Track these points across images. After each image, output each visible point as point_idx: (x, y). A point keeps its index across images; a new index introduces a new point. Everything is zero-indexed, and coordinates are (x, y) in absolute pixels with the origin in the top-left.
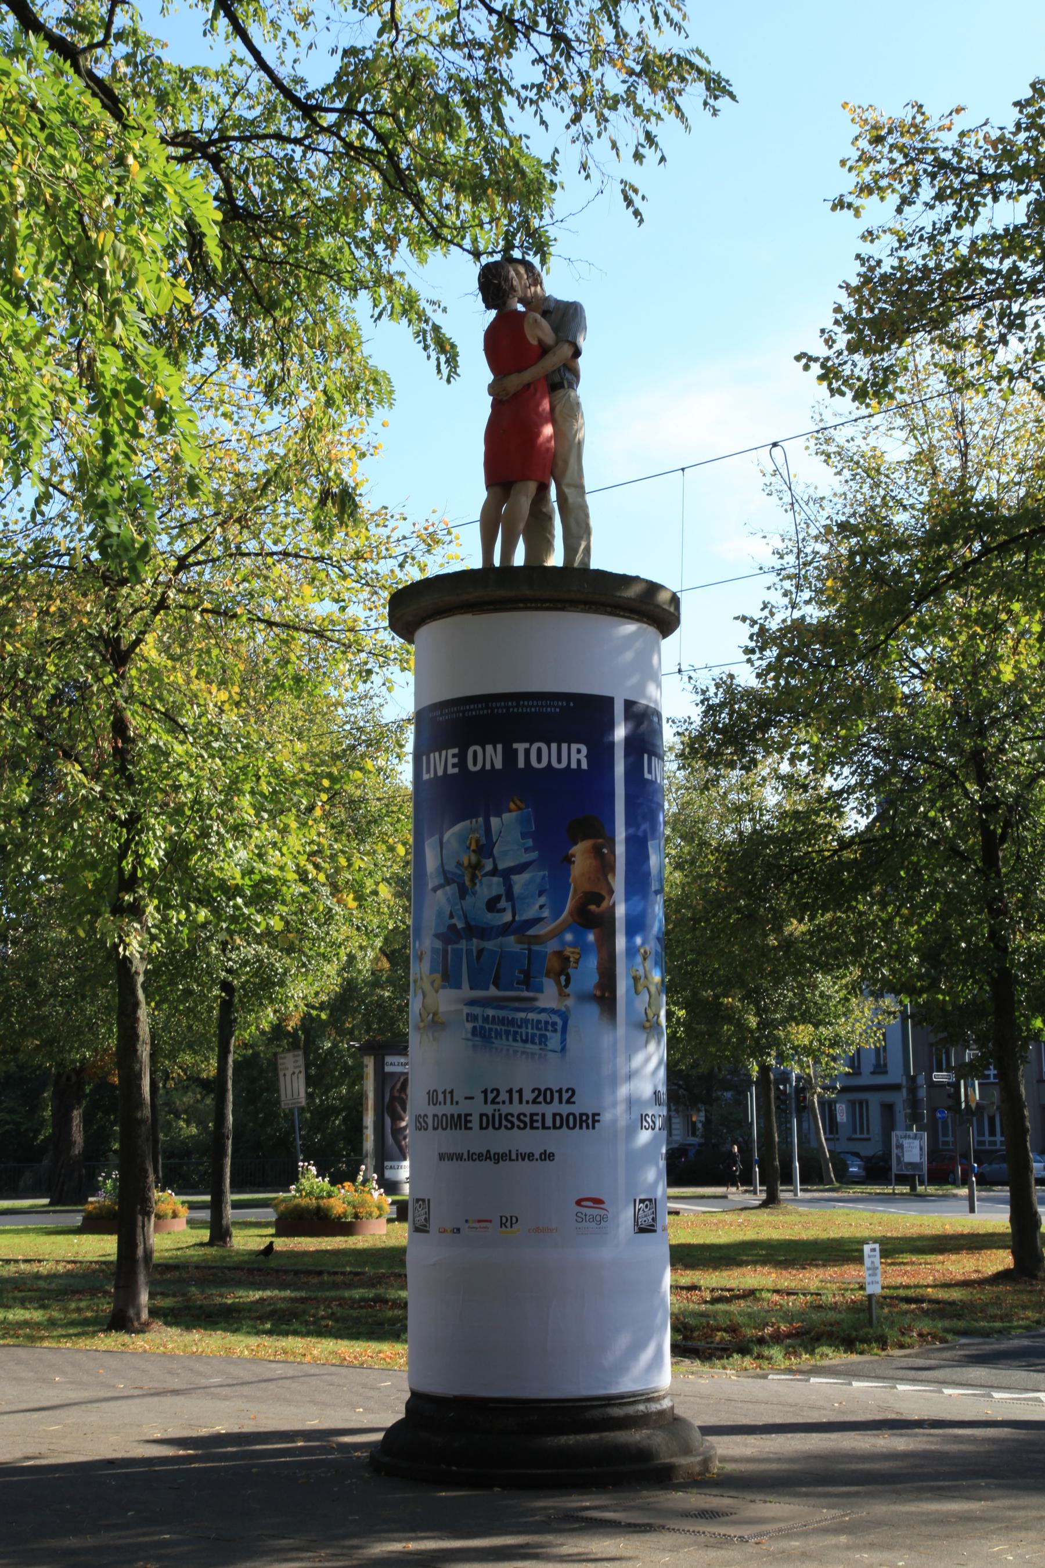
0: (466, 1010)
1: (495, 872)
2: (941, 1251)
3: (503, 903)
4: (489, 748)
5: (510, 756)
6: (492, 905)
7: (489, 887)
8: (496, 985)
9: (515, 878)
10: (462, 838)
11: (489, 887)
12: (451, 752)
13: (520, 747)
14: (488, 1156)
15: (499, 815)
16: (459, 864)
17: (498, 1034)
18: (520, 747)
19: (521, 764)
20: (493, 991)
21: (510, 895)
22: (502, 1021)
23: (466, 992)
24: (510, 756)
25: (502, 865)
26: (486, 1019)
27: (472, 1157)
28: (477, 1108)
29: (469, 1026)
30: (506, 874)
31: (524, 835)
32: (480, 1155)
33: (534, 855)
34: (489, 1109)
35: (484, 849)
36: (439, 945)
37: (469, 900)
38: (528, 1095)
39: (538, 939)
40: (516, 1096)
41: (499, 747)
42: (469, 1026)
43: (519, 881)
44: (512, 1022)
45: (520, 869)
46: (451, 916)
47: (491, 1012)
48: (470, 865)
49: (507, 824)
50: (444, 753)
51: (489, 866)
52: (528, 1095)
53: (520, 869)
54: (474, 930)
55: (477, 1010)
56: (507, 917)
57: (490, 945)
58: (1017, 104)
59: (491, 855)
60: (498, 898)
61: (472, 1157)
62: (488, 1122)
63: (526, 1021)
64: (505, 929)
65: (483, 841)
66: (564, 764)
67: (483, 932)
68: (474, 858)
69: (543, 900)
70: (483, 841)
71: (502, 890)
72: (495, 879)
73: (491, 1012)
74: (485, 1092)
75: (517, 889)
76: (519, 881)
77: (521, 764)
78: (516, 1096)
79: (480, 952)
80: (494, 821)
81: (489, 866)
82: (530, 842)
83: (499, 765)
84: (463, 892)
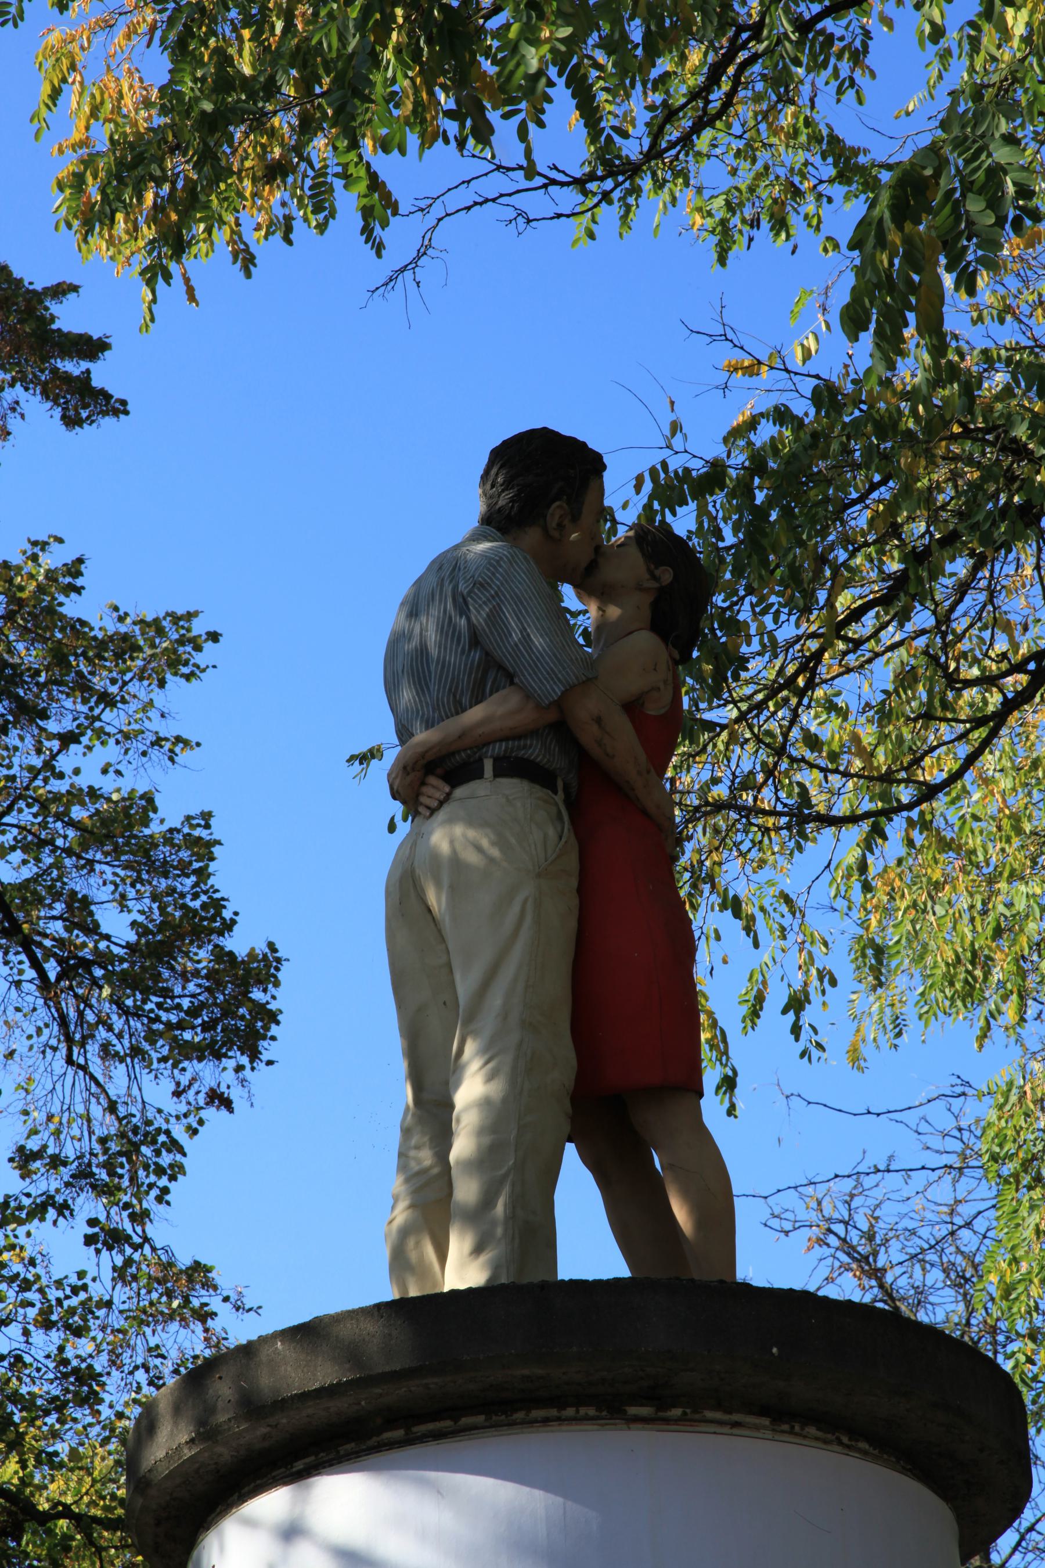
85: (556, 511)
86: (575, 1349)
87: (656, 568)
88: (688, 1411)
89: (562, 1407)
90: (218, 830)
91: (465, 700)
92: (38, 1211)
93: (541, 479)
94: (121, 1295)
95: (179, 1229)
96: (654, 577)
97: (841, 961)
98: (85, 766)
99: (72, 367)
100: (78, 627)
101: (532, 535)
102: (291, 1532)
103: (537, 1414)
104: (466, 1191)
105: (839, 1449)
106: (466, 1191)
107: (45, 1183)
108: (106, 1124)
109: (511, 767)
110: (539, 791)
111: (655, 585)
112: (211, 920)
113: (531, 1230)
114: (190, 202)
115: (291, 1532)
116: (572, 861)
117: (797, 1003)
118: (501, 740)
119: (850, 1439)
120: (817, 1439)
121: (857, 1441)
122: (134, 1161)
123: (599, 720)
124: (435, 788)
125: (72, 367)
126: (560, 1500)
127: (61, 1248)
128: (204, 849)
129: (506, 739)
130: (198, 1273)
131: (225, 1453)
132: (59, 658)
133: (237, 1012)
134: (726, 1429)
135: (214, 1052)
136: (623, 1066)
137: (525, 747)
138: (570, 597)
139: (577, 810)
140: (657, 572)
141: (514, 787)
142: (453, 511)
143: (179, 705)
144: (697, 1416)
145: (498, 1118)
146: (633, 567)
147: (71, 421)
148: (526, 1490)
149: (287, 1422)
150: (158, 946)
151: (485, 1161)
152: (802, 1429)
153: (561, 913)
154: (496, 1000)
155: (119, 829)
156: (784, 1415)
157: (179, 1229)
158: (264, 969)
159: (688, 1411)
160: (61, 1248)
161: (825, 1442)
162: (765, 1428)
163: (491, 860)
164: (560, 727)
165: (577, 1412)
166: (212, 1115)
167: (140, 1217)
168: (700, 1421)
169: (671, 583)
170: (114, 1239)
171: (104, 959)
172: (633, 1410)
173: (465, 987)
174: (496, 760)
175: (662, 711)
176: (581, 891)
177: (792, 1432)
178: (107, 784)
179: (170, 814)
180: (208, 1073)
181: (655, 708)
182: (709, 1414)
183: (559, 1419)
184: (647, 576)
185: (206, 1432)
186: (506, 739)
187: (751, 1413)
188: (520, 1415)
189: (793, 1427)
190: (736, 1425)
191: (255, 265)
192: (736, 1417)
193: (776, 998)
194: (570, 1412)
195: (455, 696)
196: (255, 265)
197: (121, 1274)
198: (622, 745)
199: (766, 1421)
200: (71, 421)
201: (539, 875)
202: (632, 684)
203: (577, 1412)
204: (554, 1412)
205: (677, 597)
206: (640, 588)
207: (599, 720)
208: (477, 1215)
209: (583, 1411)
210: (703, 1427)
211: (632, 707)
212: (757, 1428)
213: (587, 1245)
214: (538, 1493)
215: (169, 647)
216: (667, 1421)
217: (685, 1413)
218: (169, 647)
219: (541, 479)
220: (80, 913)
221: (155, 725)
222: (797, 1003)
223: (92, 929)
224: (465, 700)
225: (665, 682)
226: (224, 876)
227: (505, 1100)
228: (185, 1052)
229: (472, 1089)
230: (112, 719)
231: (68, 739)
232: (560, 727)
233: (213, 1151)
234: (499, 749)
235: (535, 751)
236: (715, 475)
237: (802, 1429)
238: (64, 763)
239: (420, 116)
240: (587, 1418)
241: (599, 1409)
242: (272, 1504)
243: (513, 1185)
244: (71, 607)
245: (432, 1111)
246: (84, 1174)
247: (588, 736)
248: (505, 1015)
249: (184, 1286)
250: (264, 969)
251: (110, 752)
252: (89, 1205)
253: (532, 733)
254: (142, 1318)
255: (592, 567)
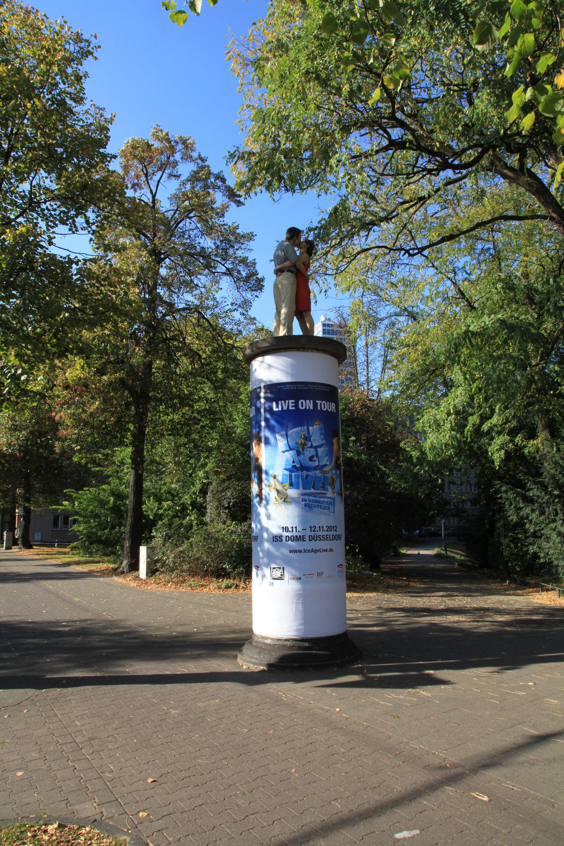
0: (302, 497)
1: (311, 447)
2: (41, 579)
3: (315, 459)
4: (308, 401)
5: (315, 405)
6: (311, 459)
7: (309, 452)
8: (314, 488)
9: (319, 449)
10: (297, 433)
11: (309, 452)
12: (291, 401)
13: (319, 402)
14: (312, 551)
15: (312, 426)
16: (297, 443)
17: (315, 506)
18: (319, 402)
19: (319, 409)
20: (312, 491)
21: (317, 456)
22: (316, 501)
23: (301, 490)
24: (315, 405)
25: (314, 445)
26: (310, 501)
27: (305, 551)
28: (308, 533)
29: (303, 503)
30: (316, 448)
31: (321, 434)
32: (309, 551)
33: (324, 442)
34: (312, 534)
35: (307, 438)
36: (287, 473)
37: (302, 457)
38: (325, 529)
39: (325, 472)
40: (294, 529)
41: (312, 401)
42: (303, 503)
43: (320, 450)
44: (319, 502)
45: (320, 446)
46: (294, 462)
47: (312, 498)
48: (302, 444)
49: (315, 430)
50: (287, 401)
51: (309, 444)
52: (325, 529)
53: (320, 446)
54: (303, 468)
55: (306, 497)
56: (317, 463)
57: (310, 473)
58: (199, 155)
59: (310, 441)
60: (313, 457)
61: (305, 551)
62: (311, 538)
63: (324, 501)
64: (316, 468)
65: (307, 435)
66: (304, 408)
67: (308, 469)
68: (303, 441)
69: (327, 458)
70: (307, 435)
71: (314, 454)
72: (312, 449)
73: (312, 498)
74: (311, 527)
75: (319, 453)
76: (320, 450)
77: (319, 409)
78: (294, 529)
79: (307, 476)
80: (310, 428)
81: (309, 444)
82: (323, 437)
83: (311, 408)
84: (299, 453)
85: (295, 237)
90: (256, 261)
92: (234, 310)
93: (293, 233)
94: (245, 321)
95: (252, 313)
97: (332, 286)
98: (239, 253)
99: (238, 199)
100: (238, 234)
101: (292, 241)
102: (262, 362)
104: (283, 322)
106: (283, 322)
107: (234, 307)
108: (243, 300)
109: (288, 271)
112: (256, 273)
113: (290, 328)
114: (250, 189)
115: (262, 362)
117: (326, 291)
122: (246, 304)
124: (279, 273)
125: (238, 199)
127: (237, 315)
128: (255, 264)
130: (254, 319)
131: (254, 353)
132: (236, 238)
133: (259, 285)
135: (256, 290)
136: (301, 307)
138: (296, 249)
139: (297, 276)
141: (289, 273)
142: (283, 236)
143: (251, 244)
145: (286, 314)
146: (305, 244)
147: (238, 206)
149: (261, 350)
150: (249, 277)
151: (285, 319)
153: (295, 289)
154: (286, 300)
155: (244, 261)
156: (318, 350)
157: (252, 313)
158: (262, 280)
160: (237, 315)
164: (295, 266)
166: (256, 298)
167: (247, 311)
170: (243, 314)
171: (242, 278)
173: (283, 298)
178: (242, 255)
179: (250, 259)
180: (255, 293)
181: (307, 263)
185: (252, 351)
193: (323, 290)
197: (245, 318)
198: (302, 268)
200: (238, 206)
202: (303, 260)
205: (310, 248)
208: (284, 325)
211: (304, 263)
213: (297, 331)
215: (250, 237)
218: (250, 237)
219: (293, 233)
220: (239, 272)
221: (248, 247)
222: (326, 291)
223: (240, 274)
226: (258, 267)
228: (253, 290)
229: (284, 311)
230: (243, 246)
231: (237, 249)
232: (295, 266)
233: (256, 304)
236: (317, 227)
238: (237, 252)
239: (278, 187)
242: (260, 359)
244: (238, 231)
245: (278, 313)
246: (240, 306)
247: (298, 267)
249: (253, 320)
250: (262, 280)
251: (243, 251)
252: (240, 310)
254: (247, 324)
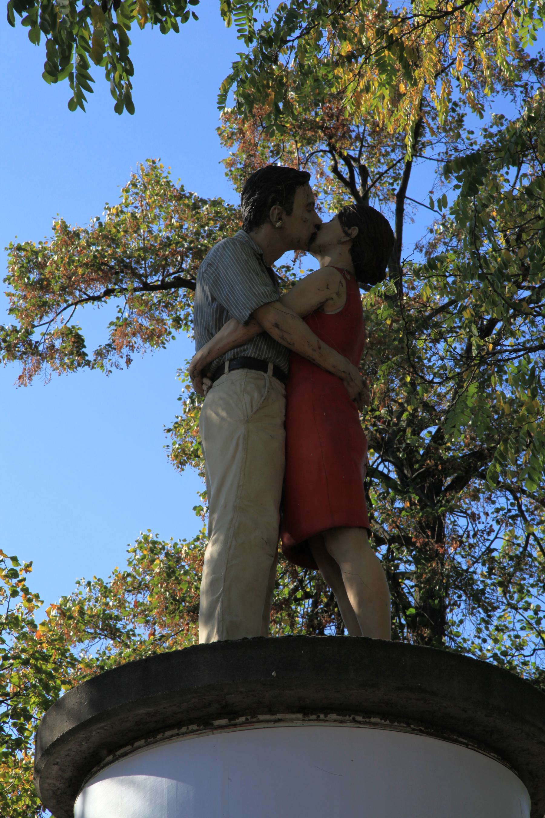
86: (160, 693)
87: (349, 229)
88: (249, 717)
89: (180, 728)
91: (213, 331)
96: (347, 234)
103: (168, 733)
105: (352, 724)
110: (253, 373)
111: (347, 239)
116: (278, 407)
118: (231, 350)
119: (364, 718)
120: (335, 721)
121: (369, 717)
123: (277, 325)
126: (174, 782)
129: (233, 348)
134: (271, 725)
137: (244, 350)
140: (349, 231)
144: (254, 720)
148: (159, 779)
152: (326, 716)
159: (249, 717)
161: (341, 722)
162: (298, 719)
163: (222, 419)
165: (188, 728)
168: (254, 722)
169: (358, 235)
172: (217, 723)
174: (231, 360)
175: (338, 311)
176: (286, 425)
177: (318, 719)
182: (261, 717)
183: (178, 735)
184: (343, 235)
186: (233, 348)
187: (293, 712)
188: (160, 736)
189: (319, 716)
190: (280, 720)
191: (484, 111)
192: (279, 716)
194: (184, 729)
195: (208, 331)
196: (484, 111)
199: (300, 716)
201: (247, 422)
203: (188, 728)
204: (176, 731)
206: (341, 243)
207: (277, 325)
209: (190, 727)
210: (257, 725)
212: (292, 720)
214: (165, 780)
216: (235, 725)
217: (247, 719)
224: (213, 331)
225: (338, 294)
227: (220, 554)
234: (230, 355)
235: (250, 351)
237: (326, 716)
240: (193, 731)
241: (199, 725)
243: (222, 602)
248: (225, 506)
253: (250, 341)
255: (313, 237)
